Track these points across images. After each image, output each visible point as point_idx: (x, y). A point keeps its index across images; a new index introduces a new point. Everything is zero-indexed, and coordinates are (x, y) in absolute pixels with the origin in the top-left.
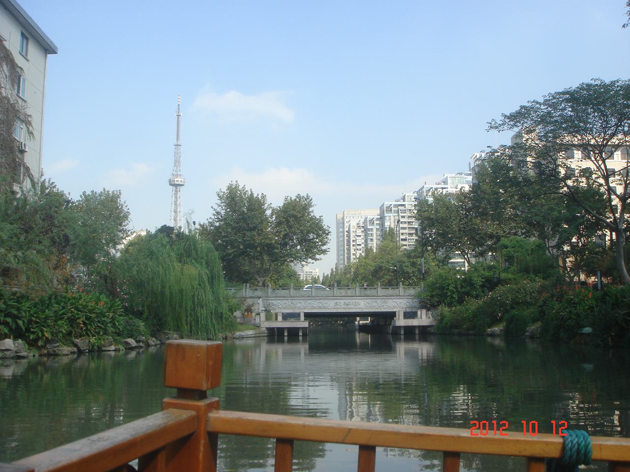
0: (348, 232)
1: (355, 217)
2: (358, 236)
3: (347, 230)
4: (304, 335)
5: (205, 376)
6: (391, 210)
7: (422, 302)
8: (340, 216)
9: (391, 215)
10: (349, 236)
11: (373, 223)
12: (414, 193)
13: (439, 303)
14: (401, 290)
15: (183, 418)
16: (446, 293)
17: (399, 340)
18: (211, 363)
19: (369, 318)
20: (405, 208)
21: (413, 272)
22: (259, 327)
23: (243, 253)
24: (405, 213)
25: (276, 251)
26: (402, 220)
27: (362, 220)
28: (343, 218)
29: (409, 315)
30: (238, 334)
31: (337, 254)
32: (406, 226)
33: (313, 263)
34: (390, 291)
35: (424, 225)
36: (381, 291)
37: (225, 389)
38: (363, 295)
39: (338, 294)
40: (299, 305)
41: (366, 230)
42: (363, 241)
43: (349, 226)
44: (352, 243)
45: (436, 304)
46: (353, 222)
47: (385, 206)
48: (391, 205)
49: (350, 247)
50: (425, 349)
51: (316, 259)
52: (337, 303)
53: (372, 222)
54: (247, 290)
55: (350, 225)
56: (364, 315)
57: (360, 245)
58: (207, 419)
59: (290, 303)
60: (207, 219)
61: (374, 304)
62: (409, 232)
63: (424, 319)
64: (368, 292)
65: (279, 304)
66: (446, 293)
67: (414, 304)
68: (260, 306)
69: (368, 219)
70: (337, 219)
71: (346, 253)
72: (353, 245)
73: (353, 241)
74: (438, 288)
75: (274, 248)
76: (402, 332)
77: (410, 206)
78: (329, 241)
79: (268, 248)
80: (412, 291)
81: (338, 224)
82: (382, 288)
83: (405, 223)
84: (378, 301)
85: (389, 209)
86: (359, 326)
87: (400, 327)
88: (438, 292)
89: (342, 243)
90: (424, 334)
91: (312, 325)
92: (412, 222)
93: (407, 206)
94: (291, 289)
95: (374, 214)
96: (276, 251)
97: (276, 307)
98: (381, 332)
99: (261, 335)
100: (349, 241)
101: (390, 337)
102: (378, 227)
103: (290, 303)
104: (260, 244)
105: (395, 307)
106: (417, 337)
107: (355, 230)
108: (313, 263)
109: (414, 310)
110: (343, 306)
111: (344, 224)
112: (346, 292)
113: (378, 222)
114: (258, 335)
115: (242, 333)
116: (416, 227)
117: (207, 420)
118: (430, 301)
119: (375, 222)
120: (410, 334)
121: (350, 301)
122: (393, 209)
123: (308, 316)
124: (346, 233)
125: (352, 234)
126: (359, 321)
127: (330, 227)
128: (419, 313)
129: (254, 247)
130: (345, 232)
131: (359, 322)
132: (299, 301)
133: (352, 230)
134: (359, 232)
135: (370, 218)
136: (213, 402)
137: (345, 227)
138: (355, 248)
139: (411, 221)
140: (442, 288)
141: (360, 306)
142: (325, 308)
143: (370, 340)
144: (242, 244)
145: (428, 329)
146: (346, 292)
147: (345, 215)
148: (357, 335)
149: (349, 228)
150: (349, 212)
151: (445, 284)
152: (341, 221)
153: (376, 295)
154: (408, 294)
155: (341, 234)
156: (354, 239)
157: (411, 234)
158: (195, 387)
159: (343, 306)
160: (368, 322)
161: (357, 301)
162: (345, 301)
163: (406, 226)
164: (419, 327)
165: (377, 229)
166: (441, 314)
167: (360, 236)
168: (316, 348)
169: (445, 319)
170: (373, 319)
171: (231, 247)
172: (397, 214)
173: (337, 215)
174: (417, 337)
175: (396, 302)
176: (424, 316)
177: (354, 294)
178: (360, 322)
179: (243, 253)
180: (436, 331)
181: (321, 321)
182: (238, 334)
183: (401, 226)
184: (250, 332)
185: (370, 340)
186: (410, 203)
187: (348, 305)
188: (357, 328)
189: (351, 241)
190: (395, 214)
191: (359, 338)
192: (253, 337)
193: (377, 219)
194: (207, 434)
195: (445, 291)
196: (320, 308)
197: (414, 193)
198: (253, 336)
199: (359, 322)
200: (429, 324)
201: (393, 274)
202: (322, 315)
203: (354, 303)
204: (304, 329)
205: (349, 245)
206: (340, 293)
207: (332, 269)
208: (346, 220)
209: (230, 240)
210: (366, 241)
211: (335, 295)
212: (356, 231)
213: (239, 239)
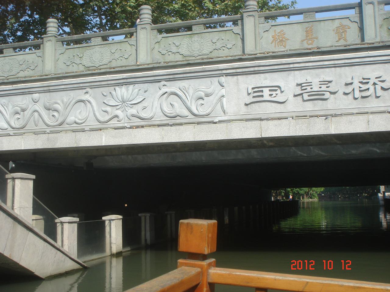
5: (206, 244)
15: (193, 273)
18: (210, 235)
37: (301, 211)
39: (267, 44)
40: (77, 115)
58: (208, 274)
59: (39, 107)
91: (341, 197)
103: (39, 107)
110: (295, 106)
112: (309, 34)
117: (208, 274)
121: (327, 74)
131: (384, 194)
132: (80, 95)
136: (211, 262)
142: (199, 120)
158: (199, 252)
159: (295, 106)
178: (387, 194)
188: (382, 203)
194: (208, 284)
196: (174, 121)
203: (356, 85)
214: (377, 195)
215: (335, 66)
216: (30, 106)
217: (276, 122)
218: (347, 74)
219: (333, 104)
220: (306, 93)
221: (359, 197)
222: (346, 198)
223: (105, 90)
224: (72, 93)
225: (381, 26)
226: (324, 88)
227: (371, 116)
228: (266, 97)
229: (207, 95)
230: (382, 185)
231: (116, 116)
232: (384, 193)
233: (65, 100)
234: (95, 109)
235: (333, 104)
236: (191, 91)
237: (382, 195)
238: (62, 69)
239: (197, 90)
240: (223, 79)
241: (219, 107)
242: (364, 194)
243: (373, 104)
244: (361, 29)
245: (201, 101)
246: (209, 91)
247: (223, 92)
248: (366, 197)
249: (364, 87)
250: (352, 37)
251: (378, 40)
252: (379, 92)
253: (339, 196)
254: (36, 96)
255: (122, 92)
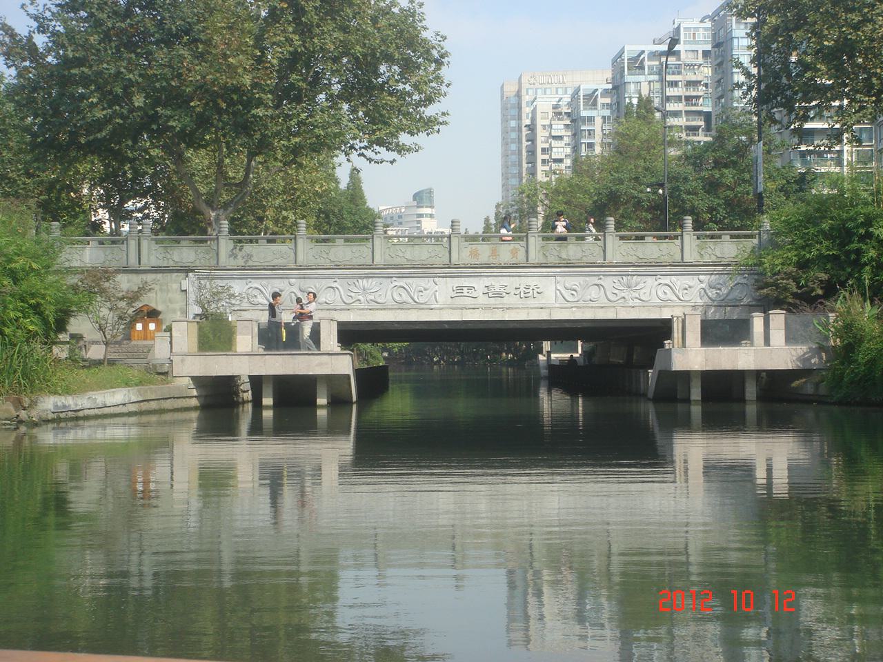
0: (532, 128)
1: (548, 91)
2: (555, 138)
3: (528, 122)
4: (339, 402)
6: (641, 67)
7: (767, 285)
8: (511, 89)
9: (641, 78)
10: (532, 139)
11: (595, 104)
12: (702, 21)
13: (830, 290)
14: (690, 243)
16: (859, 252)
17: (685, 425)
19: (580, 343)
20: (679, 59)
21: (711, 210)
22: (166, 374)
23: (149, 123)
24: (679, 73)
25: (260, 112)
26: (670, 92)
27: (567, 99)
28: (518, 95)
29: (721, 331)
30: (48, 404)
31: (503, 186)
32: (680, 107)
33: (392, 162)
34: (652, 248)
35: (766, 30)
36: (617, 248)
38: (552, 259)
41: (575, 121)
42: (568, 150)
43: (534, 112)
44: (540, 157)
45: (820, 292)
46: (543, 105)
47: (626, 57)
48: (643, 52)
49: (534, 167)
50: (775, 456)
51: (401, 149)
52: (460, 288)
53: (591, 100)
54: (145, 244)
55: (535, 109)
56: (562, 332)
57: (560, 161)
60: (23, 6)
61: (594, 293)
62: (689, 124)
63: (772, 347)
64: (572, 251)
65: (256, 292)
66: (859, 252)
67: (736, 294)
68: (179, 299)
69: (581, 94)
70: (502, 97)
71: (524, 169)
72: (544, 162)
73: (544, 150)
74: (827, 235)
75: (251, 103)
76: (696, 394)
77: (691, 55)
78: (444, 88)
79: (231, 103)
80: (729, 248)
81: (504, 109)
82: (622, 238)
83: (679, 99)
84: (608, 282)
85: (637, 64)
86: (551, 367)
87: (686, 375)
88: (825, 248)
89: (514, 158)
90: (772, 400)
91: (438, 362)
92: (698, 97)
93: (683, 56)
94: (300, 242)
95: (598, 80)
96: (260, 112)
97: (245, 305)
98: (612, 395)
99: (167, 404)
100: (532, 152)
101: (650, 412)
102: (607, 113)
104: (201, 87)
105: (665, 303)
106: (751, 410)
107: (547, 122)
108: (392, 162)
109: (735, 315)
110: (483, 300)
111: (520, 108)
112: (494, 253)
113: (608, 100)
114: (153, 405)
115: (70, 402)
116: (706, 109)
118: (798, 283)
119: (601, 101)
120: (725, 401)
121: (505, 281)
122: (647, 63)
123: (351, 335)
124: (525, 131)
125: (541, 134)
126: (549, 353)
127: (444, 38)
128: (758, 322)
129: (178, 100)
130: (524, 129)
132: (331, 283)
133: (540, 122)
134: (559, 128)
135: (586, 87)
137: (524, 116)
138: (547, 168)
139: (694, 94)
140: (842, 235)
141: (540, 301)
142: (418, 306)
143: (581, 409)
144: (142, 89)
145: (795, 384)
146: (494, 253)
147: (525, 85)
148: (543, 394)
149: (533, 119)
150: (534, 77)
151: (853, 219)
152: (514, 101)
153: (600, 261)
154: (714, 259)
155: (514, 135)
156: (546, 146)
157: (694, 129)
159: (483, 300)
160: (577, 355)
161: (532, 282)
162: (488, 282)
163: (680, 107)
164: (758, 373)
165: (604, 118)
166: (848, 327)
167: (560, 138)
168: (380, 450)
169: (866, 345)
170: (590, 345)
171: (100, 100)
172: (656, 77)
173: (502, 87)
174: (751, 410)
175: (669, 286)
176: (778, 336)
177: (521, 257)
178: (554, 356)
179: (149, 123)
180: (823, 390)
181: (462, 353)
182: (48, 404)
183: (670, 92)
184: (116, 397)
185: (581, 409)
186: (694, 47)
187: (499, 295)
188: (544, 372)
189: (539, 151)
190: (652, 78)
191: (550, 403)
192: (130, 414)
193: (606, 93)
195: (854, 246)
196: (401, 306)
197: (702, 21)
198: (133, 408)
199: (551, 354)
200: (800, 365)
201: (650, 216)
202: (354, 332)
203: (522, 289)
204: (333, 381)
205: (532, 160)
206: (475, 254)
207: (487, 220)
208: (526, 98)
209: (100, 73)
210: (576, 149)
211: (455, 259)
212: (551, 125)
213: (130, 71)
214: (537, 358)
215: (510, 276)
216: (287, 288)
217: (471, 310)
218: (516, 282)
219: (507, 300)
220: (489, 292)
221: (490, 362)
222: (454, 363)
223: (350, 281)
224: (324, 281)
225: (539, 252)
226: (502, 290)
227: (530, 310)
228: (465, 294)
229: (425, 290)
230: (547, 340)
231: (359, 300)
232: (549, 353)
233: (317, 286)
234: (342, 293)
235: (507, 300)
236: (414, 286)
237: (545, 358)
238: (312, 262)
239: (418, 286)
240: (436, 279)
241: (433, 298)
242: (504, 354)
243: (531, 302)
244: (527, 252)
245: (421, 294)
246: (427, 287)
247: (437, 288)
248: (510, 363)
249: (527, 291)
250: (521, 257)
251: (537, 261)
252: (536, 295)
253: (435, 359)
254: (293, 281)
255: (363, 283)
